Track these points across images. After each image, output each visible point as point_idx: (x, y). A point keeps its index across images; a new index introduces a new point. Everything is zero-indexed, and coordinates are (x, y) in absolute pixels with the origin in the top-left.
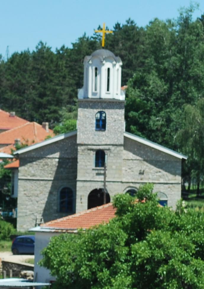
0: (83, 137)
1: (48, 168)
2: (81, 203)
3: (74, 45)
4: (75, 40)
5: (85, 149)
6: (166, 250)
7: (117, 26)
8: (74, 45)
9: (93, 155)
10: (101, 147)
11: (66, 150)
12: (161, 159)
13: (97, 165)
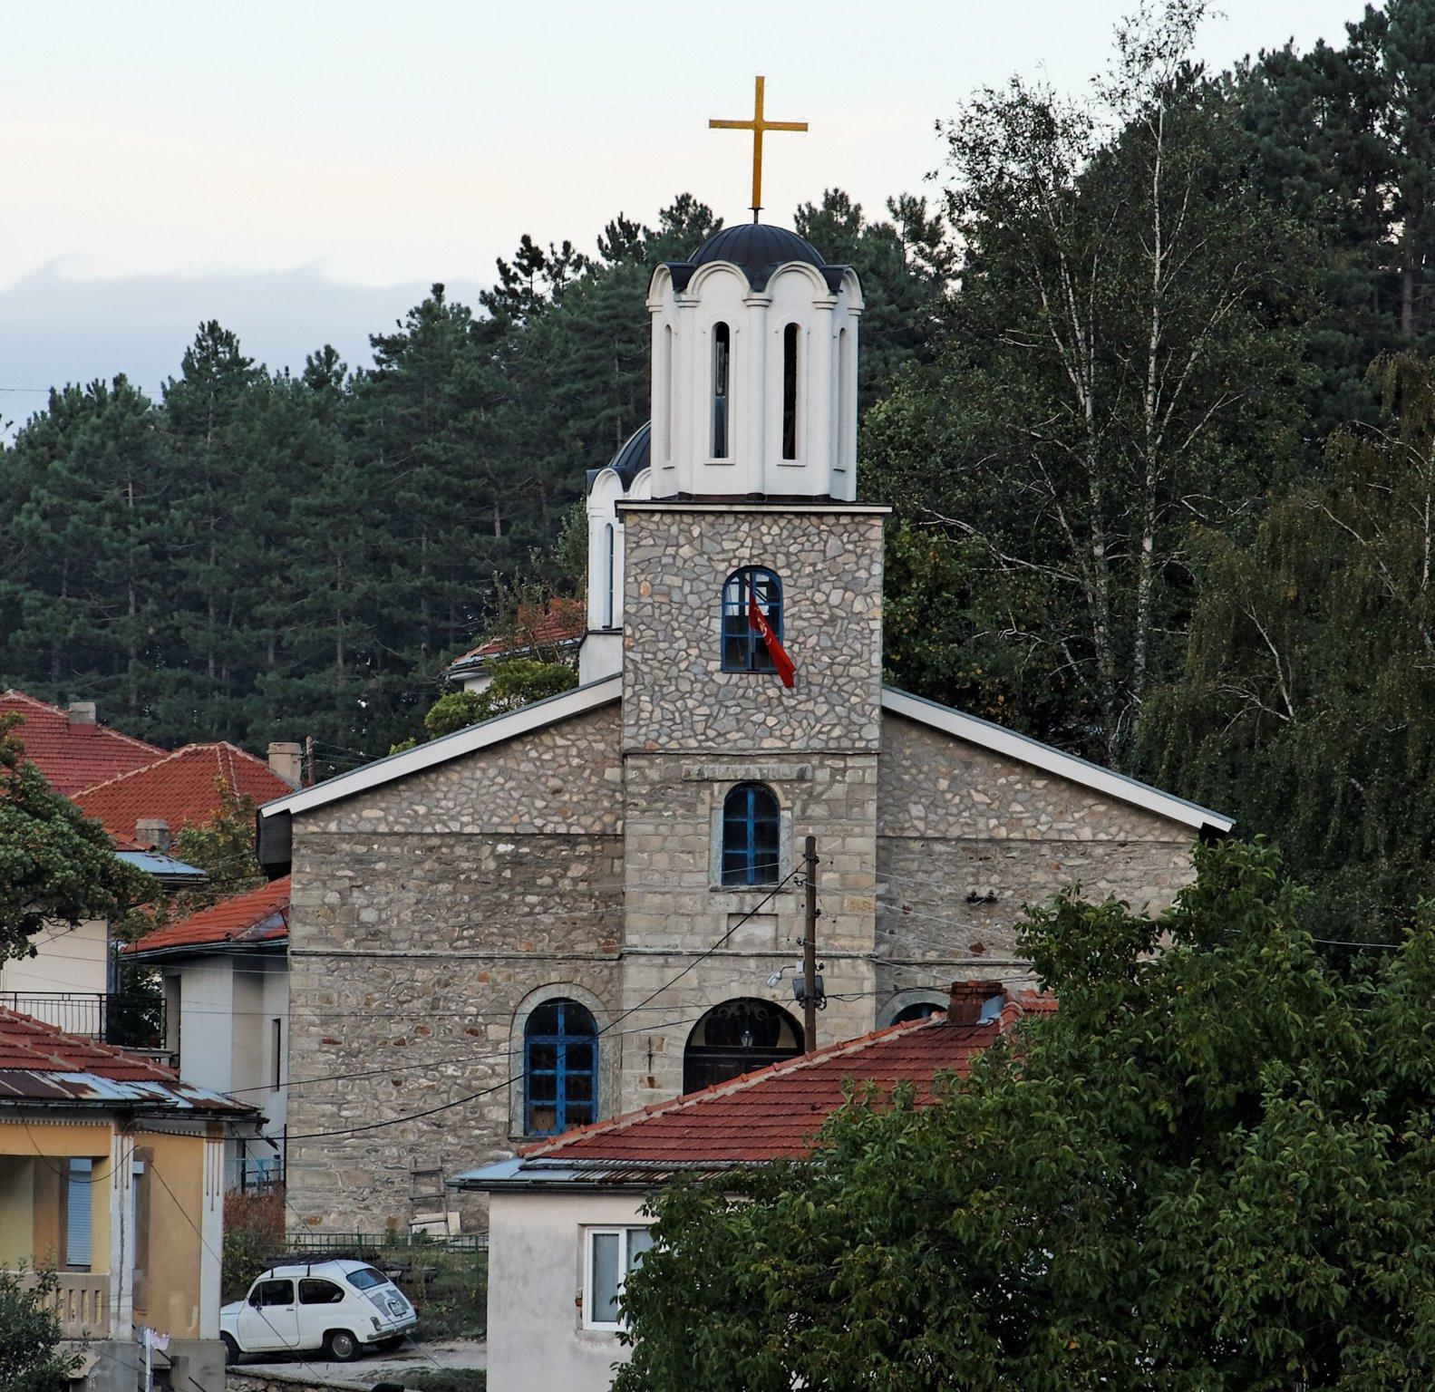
0: (657, 714)
1: (454, 892)
2: (651, 1081)
3: (801, 217)
4: (393, 320)
5: (666, 783)
6: (1089, 429)
7: (215, 358)
8: (390, 346)
9: (799, 633)
10: (753, 771)
11: (557, 791)
12: (1086, 834)
13: (733, 870)
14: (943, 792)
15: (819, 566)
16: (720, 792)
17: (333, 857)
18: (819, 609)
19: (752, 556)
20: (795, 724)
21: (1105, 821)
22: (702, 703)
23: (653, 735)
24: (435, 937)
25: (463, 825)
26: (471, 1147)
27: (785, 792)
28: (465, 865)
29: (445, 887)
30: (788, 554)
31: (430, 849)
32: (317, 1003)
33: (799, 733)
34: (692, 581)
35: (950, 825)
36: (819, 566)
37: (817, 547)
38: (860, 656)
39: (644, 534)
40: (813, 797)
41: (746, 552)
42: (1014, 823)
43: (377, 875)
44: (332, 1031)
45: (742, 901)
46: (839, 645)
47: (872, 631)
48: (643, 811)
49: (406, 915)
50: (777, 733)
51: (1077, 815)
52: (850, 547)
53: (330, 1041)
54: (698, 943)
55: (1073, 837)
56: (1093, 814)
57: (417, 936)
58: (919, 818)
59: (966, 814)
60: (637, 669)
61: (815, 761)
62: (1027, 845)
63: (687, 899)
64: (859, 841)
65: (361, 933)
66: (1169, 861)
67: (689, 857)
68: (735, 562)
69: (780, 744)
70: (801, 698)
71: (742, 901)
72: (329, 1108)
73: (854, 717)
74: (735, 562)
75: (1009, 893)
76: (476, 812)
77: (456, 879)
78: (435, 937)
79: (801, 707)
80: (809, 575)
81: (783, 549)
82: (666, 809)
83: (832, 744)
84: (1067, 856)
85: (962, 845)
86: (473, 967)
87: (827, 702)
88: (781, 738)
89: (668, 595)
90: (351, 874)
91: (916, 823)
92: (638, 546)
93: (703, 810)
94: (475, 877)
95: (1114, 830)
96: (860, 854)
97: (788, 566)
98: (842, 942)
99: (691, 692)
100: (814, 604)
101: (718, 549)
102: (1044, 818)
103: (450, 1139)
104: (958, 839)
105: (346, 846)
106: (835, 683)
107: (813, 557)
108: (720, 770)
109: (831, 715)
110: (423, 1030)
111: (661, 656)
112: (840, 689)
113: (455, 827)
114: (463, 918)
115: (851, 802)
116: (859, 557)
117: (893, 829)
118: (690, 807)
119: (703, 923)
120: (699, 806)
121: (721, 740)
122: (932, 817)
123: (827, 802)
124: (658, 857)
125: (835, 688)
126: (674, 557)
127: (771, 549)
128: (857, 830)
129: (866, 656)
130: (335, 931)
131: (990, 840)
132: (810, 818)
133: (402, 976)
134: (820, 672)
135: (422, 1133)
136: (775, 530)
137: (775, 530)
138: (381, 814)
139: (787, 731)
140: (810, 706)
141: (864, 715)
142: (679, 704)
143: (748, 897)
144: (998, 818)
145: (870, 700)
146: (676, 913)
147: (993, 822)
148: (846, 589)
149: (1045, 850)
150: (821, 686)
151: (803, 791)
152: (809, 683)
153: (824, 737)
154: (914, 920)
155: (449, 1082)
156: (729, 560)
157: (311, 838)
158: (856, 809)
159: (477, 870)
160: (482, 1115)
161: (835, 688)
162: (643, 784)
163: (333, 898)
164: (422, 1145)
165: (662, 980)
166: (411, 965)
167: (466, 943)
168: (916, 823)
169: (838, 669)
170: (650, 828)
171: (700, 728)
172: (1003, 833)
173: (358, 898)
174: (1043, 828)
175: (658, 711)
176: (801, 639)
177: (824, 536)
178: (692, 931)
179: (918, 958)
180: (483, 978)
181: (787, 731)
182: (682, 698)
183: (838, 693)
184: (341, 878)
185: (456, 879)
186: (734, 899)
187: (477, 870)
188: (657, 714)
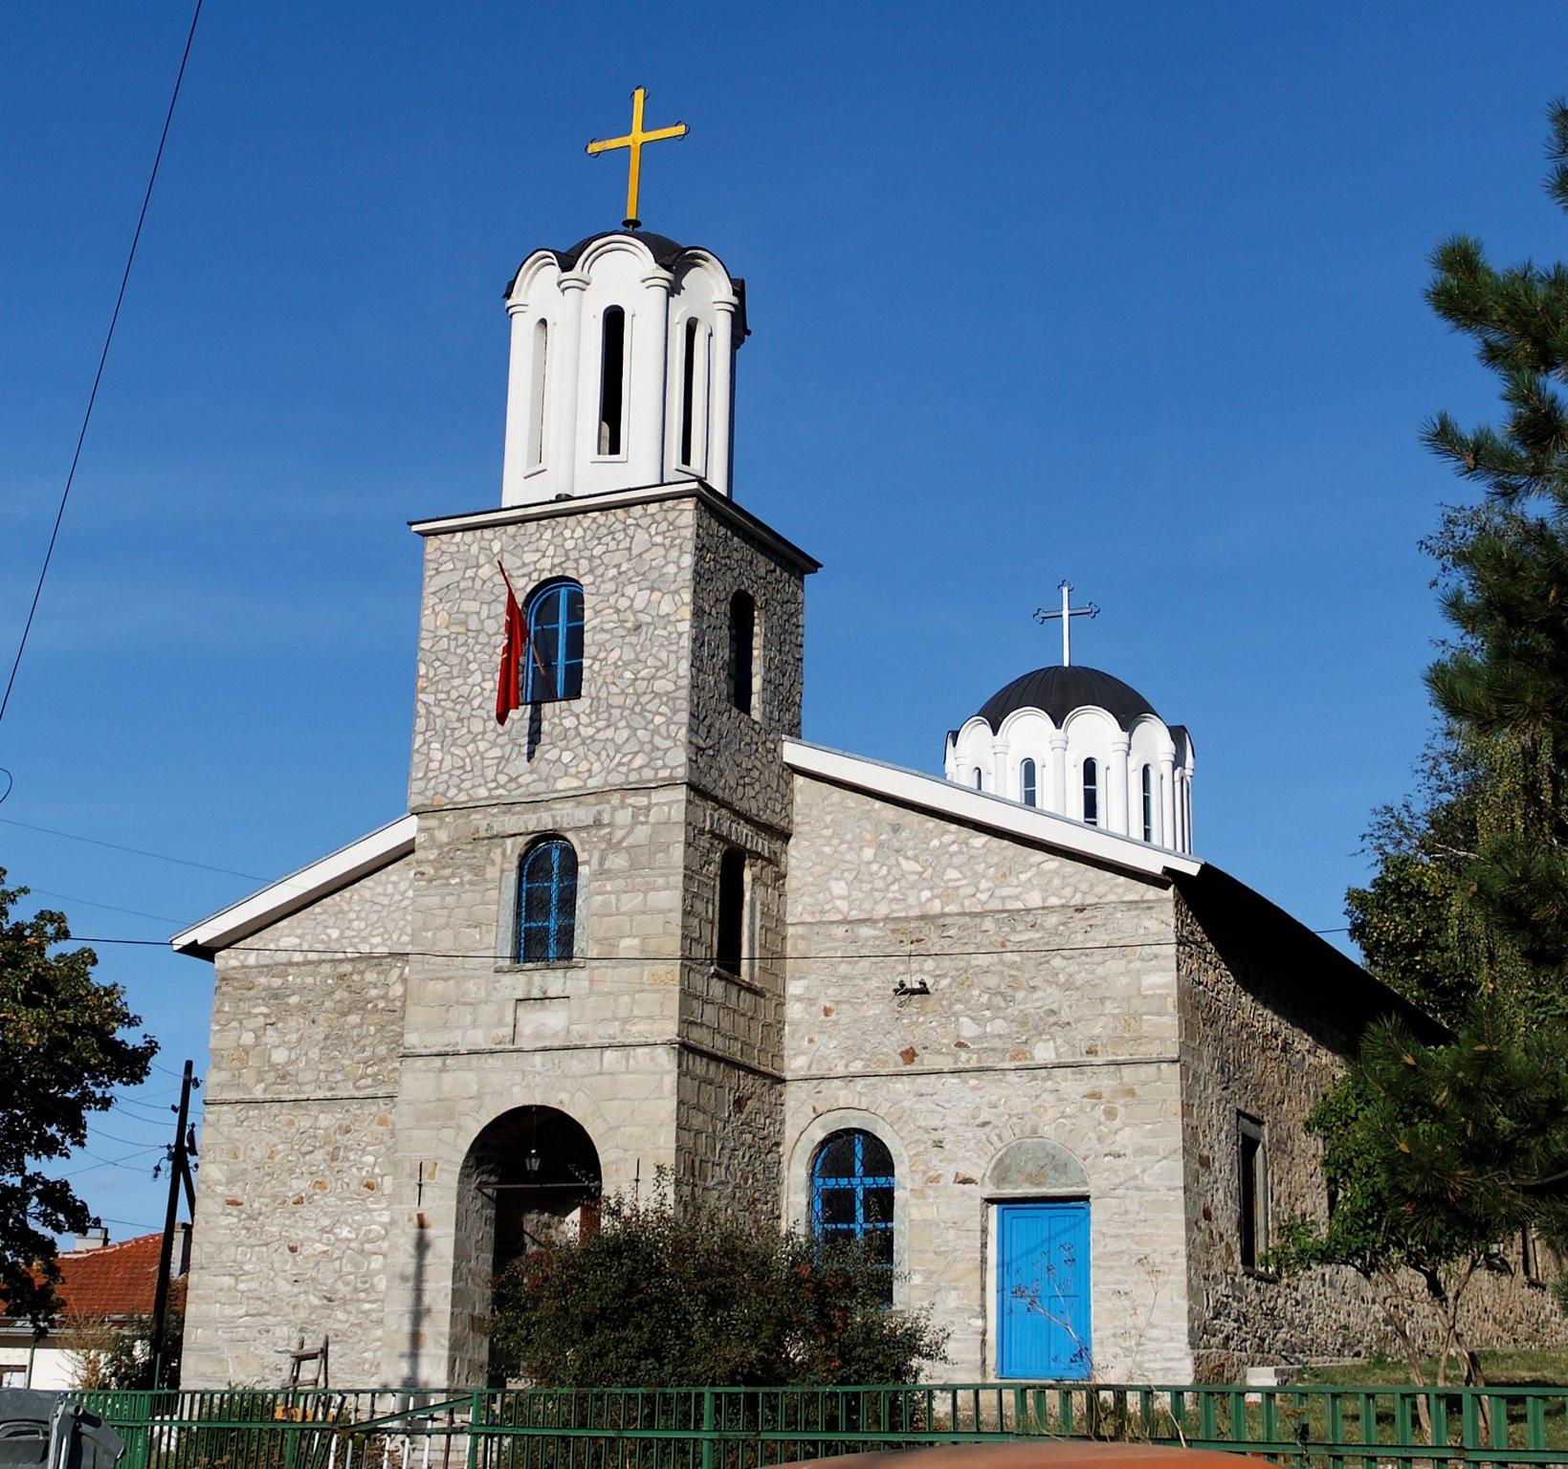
0: (447, 764)
12: (1034, 899)
14: (869, 863)
15: (624, 568)
16: (514, 848)
17: (251, 993)
18: (622, 616)
19: (554, 566)
20: (592, 757)
21: (1056, 882)
22: (494, 744)
23: (442, 788)
24: (339, 1077)
25: (372, 946)
26: (359, 1325)
27: (582, 842)
28: (373, 992)
29: (354, 1019)
30: (591, 558)
31: (342, 977)
32: (225, 1158)
33: (596, 767)
34: (489, 604)
35: (876, 903)
36: (624, 568)
37: (622, 546)
38: (666, 666)
39: (445, 558)
40: (613, 846)
41: (547, 563)
42: (949, 893)
43: (289, 1011)
44: (236, 1192)
45: (530, 983)
46: (642, 656)
47: (680, 635)
48: (430, 881)
49: (314, 1054)
50: (573, 771)
51: (1023, 877)
52: (658, 539)
53: (234, 1203)
54: (478, 1038)
55: (1019, 905)
56: (1040, 874)
57: (322, 1076)
58: (840, 898)
59: (895, 887)
60: (429, 712)
61: (615, 799)
62: (967, 919)
63: (470, 985)
64: (664, 894)
65: (270, 1077)
66: (1138, 925)
67: (475, 933)
68: (535, 576)
69: (576, 783)
70: (601, 724)
71: (530, 983)
72: (228, 1281)
73: (658, 740)
74: (535, 576)
75: (945, 982)
76: (386, 931)
77: (363, 1009)
78: (339, 1077)
79: (601, 736)
80: (612, 579)
81: (587, 553)
82: (453, 875)
83: (634, 776)
84: (1013, 930)
85: (891, 926)
86: (374, 1109)
87: (629, 726)
88: (576, 776)
89: (464, 623)
90: (265, 1010)
91: (838, 903)
92: (438, 572)
93: (492, 873)
94: (382, 1004)
95: (1068, 892)
96: (662, 912)
97: (591, 571)
98: (641, 1027)
99: (484, 733)
100: (618, 611)
101: (519, 563)
102: (984, 884)
103: (340, 1315)
104: (886, 919)
105: (263, 980)
106: (638, 703)
107: (618, 557)
108: (510, 823)
109: (633, 741)
110: (321, 1185)
111: (454, 694)
112: (643, 710)
113: (365, 949)
114: (367, 1054)
115: (656, 846)
116: (667, 551)
117: (813, 914)
118: (478, 870)
119: (487, 1012)
120: (489, 868)
121: (513, 785)
122: (856, 894)
123: (628, 849)
124: (442, 935)
125: (638, 709)
126: (473, 579)
127: (573, 555)
128: (661, 881)
129: (672, 666)
130: (248, 1076)
131: (923, 917)
132: (609, 871)
133: (305, 1123)
134: (623, 692)
135: (313, 1308)
136: (579, 532)
137: (579, 532)
138: (297, 941)
139: (584, 766)
140: (610, 733)
141: (668, 737)
142: (471, 748)
143: (536, 975)
144: (931, 889)
145: (676, 718)
146: (458, 1002)
147: (926, 894)
148: (652, 589)
149: (988, 924)
150: (622, 707)
151: (601, 839)
152: (610, 706)
153: (624, 769)
154: (836, 1023)
155: (343, 1246)
156: (529, 575)
157: (232, 973)
158: (660, 855)
159: (384, 997)
160: (372, 1286)
161: (638, 709)
162: (431, 848)
163: (248, 1038)
164: (312, 1323)
165: (439, 1087)
166: (314, 1109)
167: (369, 1081)
168: (838, 903)
169: (641, 686)
170: (436, 900)
171: (490, 773)
172: (936, 907)
173: (271, 1037)
174: (983, 897)
175: (448, 757)
176: (602, 656)
177: (630, 532)
178: (474, 1025)
179: (840, 1070)
180: (382, 1122)
181: (584, 766)
182: (473, 741)
183: (640, 714)
184: (256, 1015)
185: (363, 1009)
186: (521, 978)
187: (384, 997)
188: (447, 764)
